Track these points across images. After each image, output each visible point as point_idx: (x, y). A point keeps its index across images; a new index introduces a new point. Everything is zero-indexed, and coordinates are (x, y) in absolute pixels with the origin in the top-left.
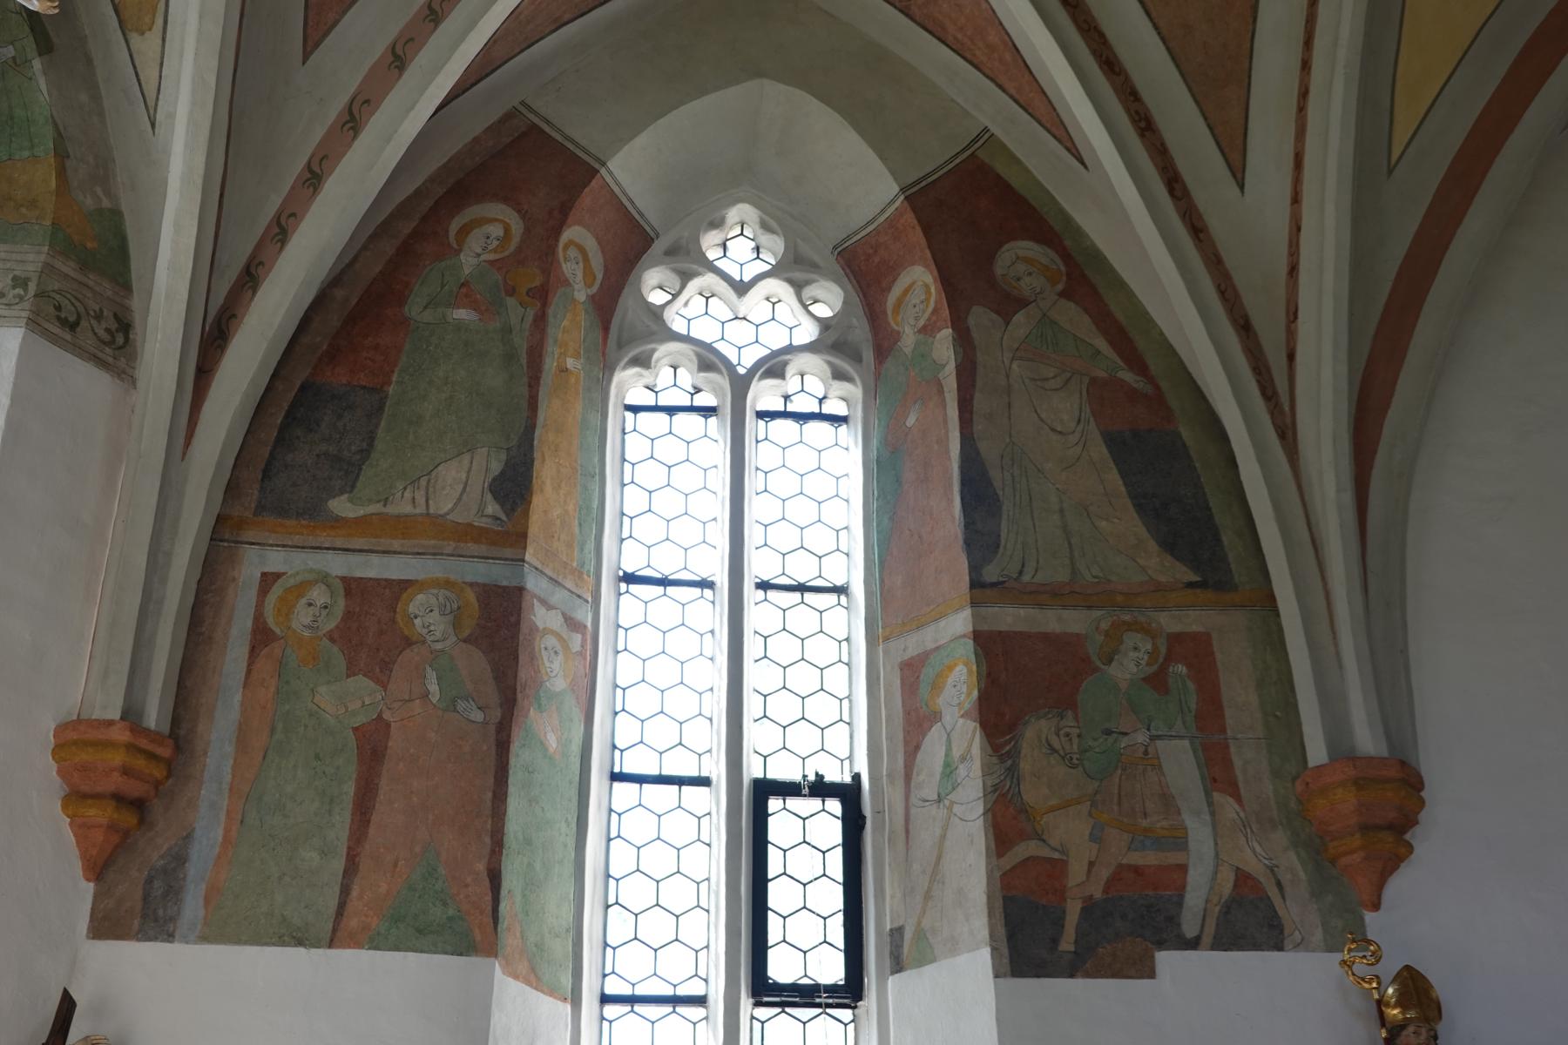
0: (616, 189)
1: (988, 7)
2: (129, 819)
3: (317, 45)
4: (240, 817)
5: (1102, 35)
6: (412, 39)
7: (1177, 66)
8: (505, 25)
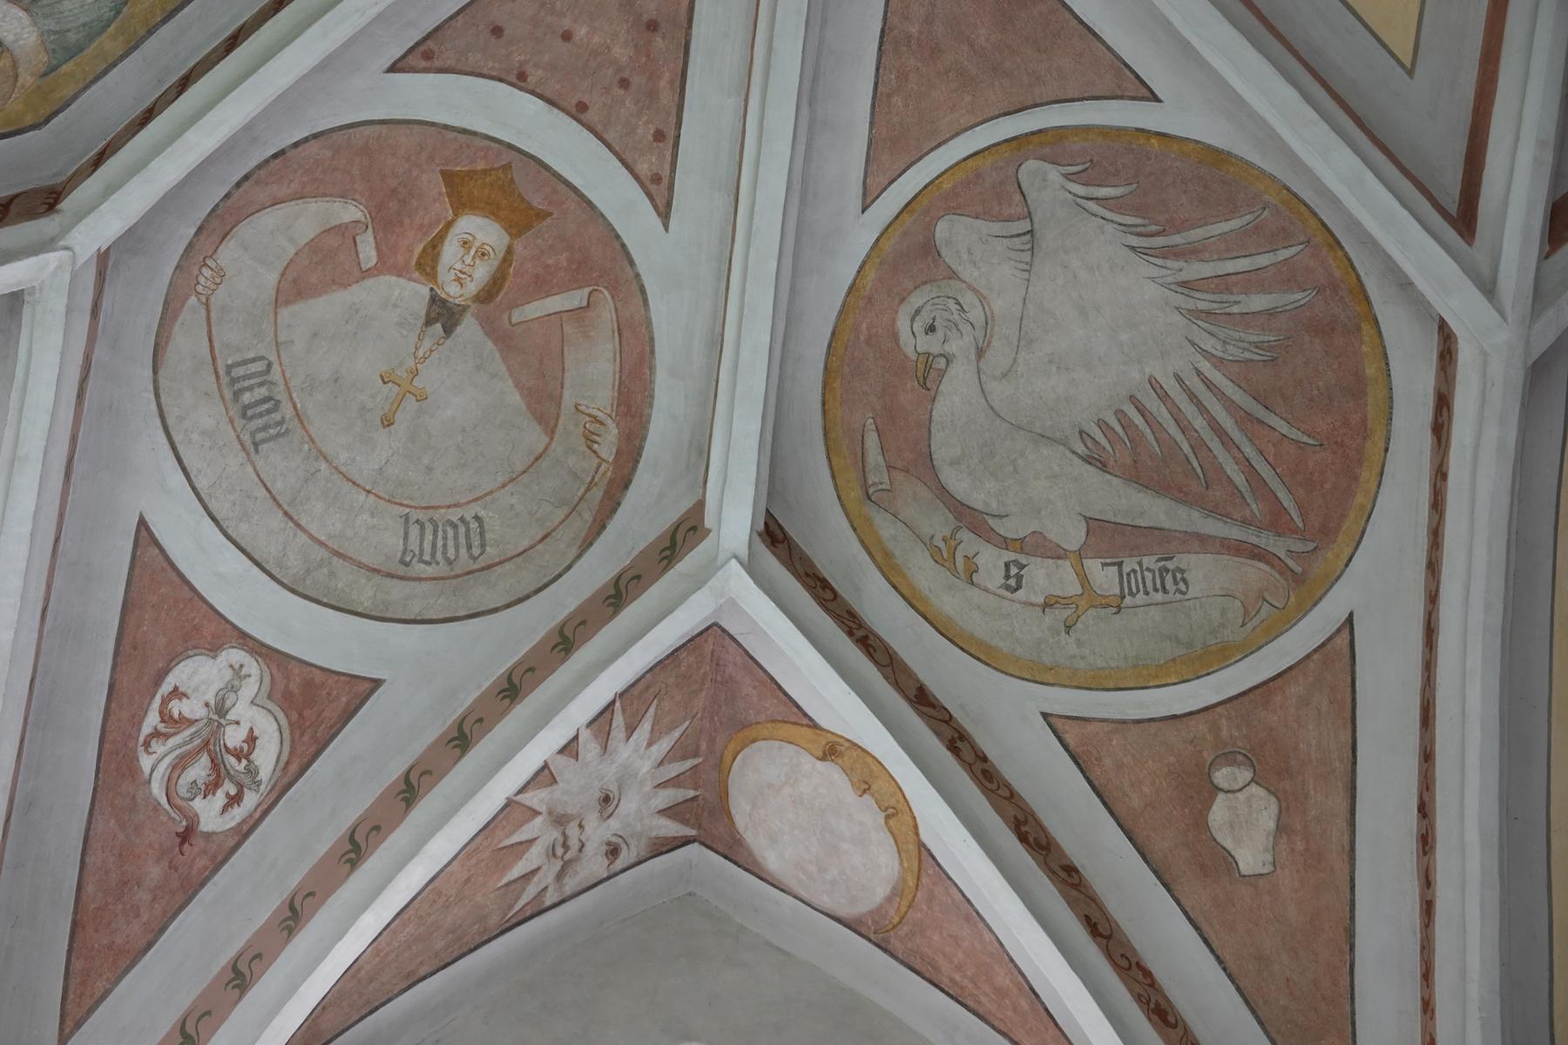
1: (994, 939)
2: (1026, 275)
3: (78, 1025)
4: (928, 484)
5: (1147, 973)
6: (208, 1013)
7: (1253, 1012)
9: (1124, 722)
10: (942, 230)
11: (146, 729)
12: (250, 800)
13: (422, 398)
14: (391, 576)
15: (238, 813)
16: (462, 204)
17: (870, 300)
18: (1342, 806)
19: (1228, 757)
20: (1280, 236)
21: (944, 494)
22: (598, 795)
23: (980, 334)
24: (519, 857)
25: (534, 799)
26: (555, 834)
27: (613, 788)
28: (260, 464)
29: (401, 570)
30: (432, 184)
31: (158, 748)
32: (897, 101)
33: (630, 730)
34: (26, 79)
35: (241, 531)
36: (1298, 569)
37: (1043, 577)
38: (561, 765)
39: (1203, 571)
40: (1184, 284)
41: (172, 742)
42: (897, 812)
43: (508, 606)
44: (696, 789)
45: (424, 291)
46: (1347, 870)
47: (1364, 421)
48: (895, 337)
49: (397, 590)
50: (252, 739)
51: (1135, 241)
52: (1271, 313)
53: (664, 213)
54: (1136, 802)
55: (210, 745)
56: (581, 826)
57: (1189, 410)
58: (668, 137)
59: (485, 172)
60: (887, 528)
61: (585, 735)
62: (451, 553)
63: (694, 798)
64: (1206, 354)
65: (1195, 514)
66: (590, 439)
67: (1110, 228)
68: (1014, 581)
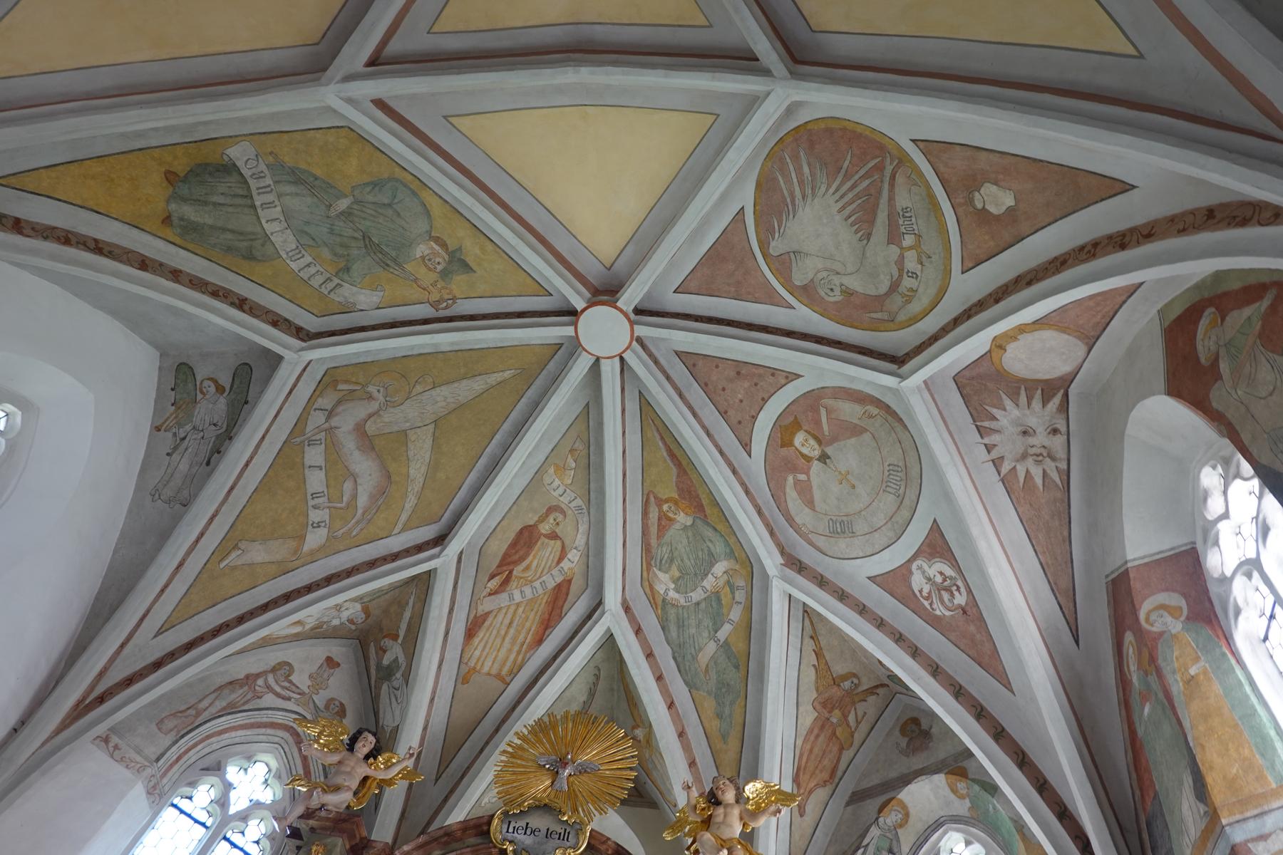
0: (1146, 560)
3: (1010, 683)
7: (1069, 214)
8: (1049, 574)
9: (962, 242)
10: (798, 283)
11: (928, 607)
12: (960, 583)
13: (848, 473)
14: (901, 503)
15: (963, 589)
16: (791, 444)
17: (825, 310)
18: (984, 153)
19: (971, 201)
20: (782, 160)
21: (888, 294)
22: (1020, 437)
23: (831, 273)
24: (1032, 478)
25: (1006, 468)
26: (1030, 460)
27: (1020, 429)
28: (858, 534)
29: (901, 498)
30: (784, 451)
31: (935, 606)
32: (757, 295)
33: (994, 418)
34: (737, 567)
35: (878, 548)
36: (897, 161)
37: (911, 263)
38: (995, 454)
39: (902, 201)
40: (803, 198)
41: (934, 601)
42: (1022, 329)
43: (921, 463)
44: (1037, 389)
45: (816, 462)
46: (1009, 157)
47: (841, 129)
48: (836, 303)
49: (906, 502)
50: (941, 573)
51: (791, 216)
52: (809, 164)
53: (799, 376)
54: (992, 243)
55: (940, 588)
56: (1032, 447)
57: (846, 199)
58: (774, 372)
59: (781, 434)
60: (902, 317)
61: (986, 441)
62: (898, 479)
63: (1042, 390)
64: (827, 190)
65: (882, 201)
66: (871, 417)
67: (788, 225)
68: (914, 275)
